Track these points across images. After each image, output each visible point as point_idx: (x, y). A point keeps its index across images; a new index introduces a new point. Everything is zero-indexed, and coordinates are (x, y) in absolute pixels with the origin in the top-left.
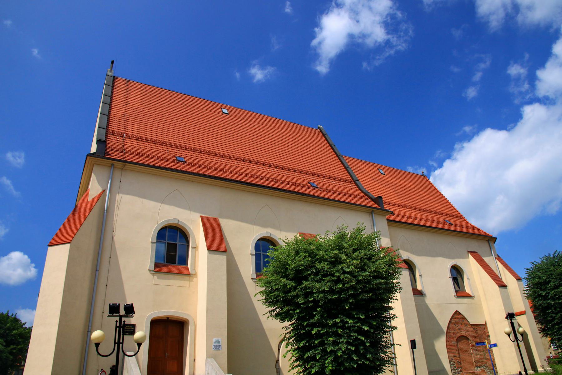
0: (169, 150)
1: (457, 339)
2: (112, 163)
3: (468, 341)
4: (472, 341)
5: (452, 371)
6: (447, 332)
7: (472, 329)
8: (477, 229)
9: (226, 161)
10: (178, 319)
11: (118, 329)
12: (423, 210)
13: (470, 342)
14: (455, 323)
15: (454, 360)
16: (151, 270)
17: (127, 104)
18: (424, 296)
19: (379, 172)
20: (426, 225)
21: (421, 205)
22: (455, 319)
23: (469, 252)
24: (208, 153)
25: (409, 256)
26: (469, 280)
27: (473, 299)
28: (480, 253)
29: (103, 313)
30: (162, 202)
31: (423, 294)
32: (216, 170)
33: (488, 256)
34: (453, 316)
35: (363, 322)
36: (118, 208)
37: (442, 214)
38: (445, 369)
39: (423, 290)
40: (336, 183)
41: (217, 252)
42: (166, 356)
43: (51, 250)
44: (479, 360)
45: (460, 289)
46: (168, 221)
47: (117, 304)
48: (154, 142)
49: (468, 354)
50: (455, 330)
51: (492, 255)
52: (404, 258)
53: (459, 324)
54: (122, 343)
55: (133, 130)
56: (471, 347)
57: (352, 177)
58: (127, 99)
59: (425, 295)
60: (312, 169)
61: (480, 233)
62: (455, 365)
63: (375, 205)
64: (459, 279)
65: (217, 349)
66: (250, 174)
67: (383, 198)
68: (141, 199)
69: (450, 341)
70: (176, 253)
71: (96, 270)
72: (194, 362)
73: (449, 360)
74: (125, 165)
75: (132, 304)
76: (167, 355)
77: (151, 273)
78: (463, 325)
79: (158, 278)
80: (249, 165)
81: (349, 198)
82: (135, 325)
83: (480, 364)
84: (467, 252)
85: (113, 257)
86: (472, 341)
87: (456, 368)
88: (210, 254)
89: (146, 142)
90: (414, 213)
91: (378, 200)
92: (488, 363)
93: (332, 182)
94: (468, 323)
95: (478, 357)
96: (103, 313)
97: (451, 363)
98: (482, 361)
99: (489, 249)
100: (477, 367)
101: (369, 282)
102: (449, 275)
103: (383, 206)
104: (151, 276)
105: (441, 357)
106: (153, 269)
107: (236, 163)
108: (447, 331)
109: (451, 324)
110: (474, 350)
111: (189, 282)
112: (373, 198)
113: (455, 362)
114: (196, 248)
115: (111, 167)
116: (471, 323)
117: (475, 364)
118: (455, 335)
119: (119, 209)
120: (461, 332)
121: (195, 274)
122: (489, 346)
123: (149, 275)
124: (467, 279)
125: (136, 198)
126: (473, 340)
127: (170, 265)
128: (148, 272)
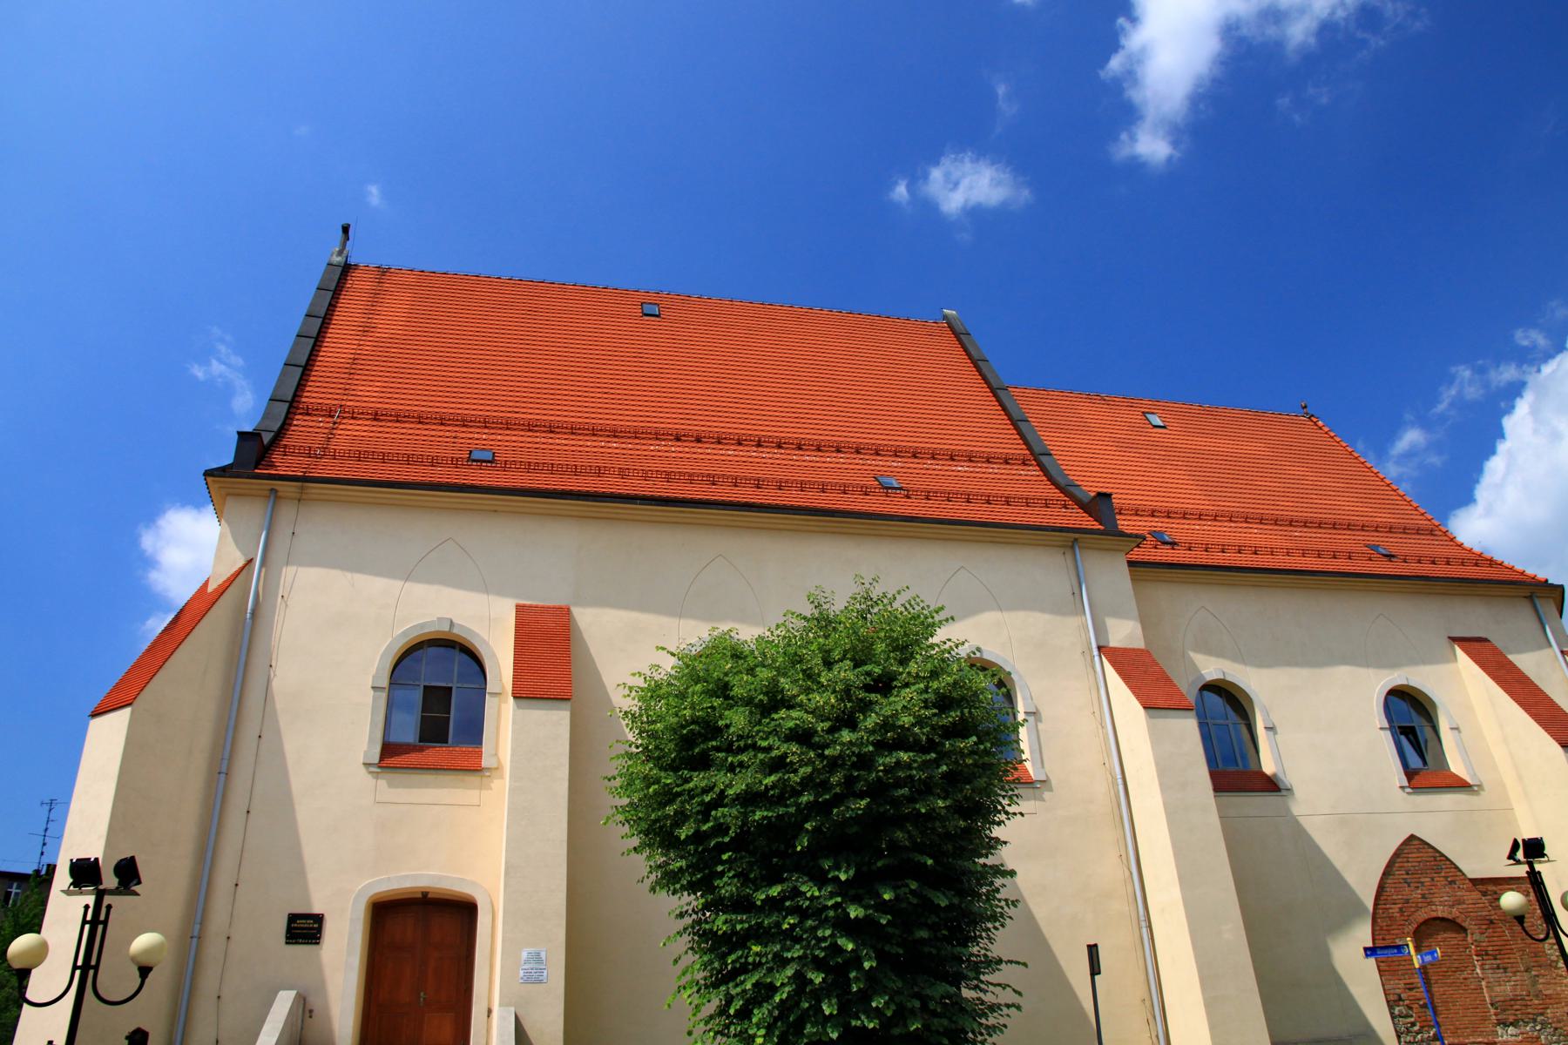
0: (458, 434)
1: (1417, 928)
2: (270, 487)
3: (1463, 935)
4: (1477, 936)
5: (1399, 1037)
6: (1375, 909)
7: (1476, 895)
8: (1491, 562)
9: (624, 446)
10: (460, 897)
11: (87, 927)
12: (1405, 529)
13: (1469, 938)
14: (1405, 876)
15: (1407, 1002)
16: (370, 764)
17: (366, 330)
18: (1284, 793)
19: (1146, 421)
20: (1294, 566)
21: (1287, 508)
22: (1406, 864)
23: (1454, 640)
24: (573, 430)
25: (1225, 670)
26: (1460, 732)
27: (1476, 793)
28: (1498, 641)
29: (237, 885)
30: (408, 578)
31: (1281, 786)
32: (576, 471)
33: (1532, 650)
34: (1397, 855)
35: (850, 891)
36: (286, 602)
37: (1363, 528)
38: (1373, 1031)
39: (1281, 776)
40: (972, 469)
41: (550, 702)
42: (422, 999)
43: (95, 724)
44: (1511, 1000)
45: (1425, 763)
46: (422, 626)
47: (90, 859)
48: (420, 420)
49: (1465, 979)
50: (1407, 901)
51: (1550, 645)
52: (1209, 678)
53: (1422, 880)
54: (96, 968)
55: (368, 394)
56: (1477, 955)
57: (1029, 448)
58: (371, 316)
59: (1289, 790)
60: (1271, 471)
61: (1502, 577)
62: (1412, 1016)
63: (1089, 523)
64: (1425, 732)
65: (534, 979)
66: (373, 452)
67: (1113, 496)
68: (349, 575)
69: (1387, 937)
70: (449, 713)
71: (221, 770)
72: (488, 1016)
73: (1388, 1002)
74: (302, 488)
75: (133, 858)
76: (424, 998)
77: (370, 772)
78: (1440, 881)
79: (390, 785)
80: (692, 450)
81: (405, 468)
82: (323, 915)
83: (1515, 1015)
84: (1446, 642)
85: (269, 735)
86: (1477, 936)
87: (1416, 1028)
88: (519, 707)
89: (636, 438)
90: (1255, 535)
91: (1100, 505)
92: (1549, 1011)
93: (960, 469)
94: (1459, 873)
95: (1507, 989)
96: (237, 885)
97: (1396, 1012)
98: (1523, 1003)
99: (1537, 626)
100: (1505, 1024)
101: (865, 762)
102: (1379, 719)
103: (1116, 520)
104: (370, 780)
105: (1355, 990)
106: (377, 761)
107: (652, 448)
108: (1376, 904)
109: (1389, 881)
110: (1487, 967)
111: (477, 792)
112: (1086, 500)
113: (1411, 1008)
114: (500, 694)
115: (269, 497)
116: (1470, 876)
117: (1496, 1014)
118: (1409, 916)
119: (287, 605)
120: (1433, 907)
121: (497, 769)
122: (1418, 959)
123: (364, 779)
124: (1450, 731)
125: (335, 574)
126: (1482, 933)
127: (428, 747)
128: (363, 770)
